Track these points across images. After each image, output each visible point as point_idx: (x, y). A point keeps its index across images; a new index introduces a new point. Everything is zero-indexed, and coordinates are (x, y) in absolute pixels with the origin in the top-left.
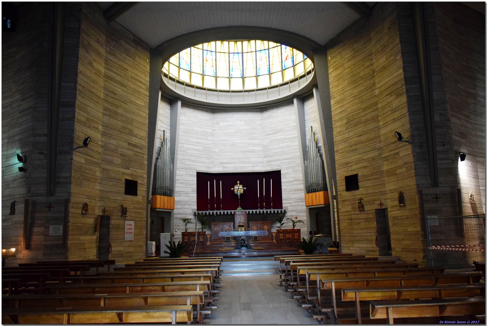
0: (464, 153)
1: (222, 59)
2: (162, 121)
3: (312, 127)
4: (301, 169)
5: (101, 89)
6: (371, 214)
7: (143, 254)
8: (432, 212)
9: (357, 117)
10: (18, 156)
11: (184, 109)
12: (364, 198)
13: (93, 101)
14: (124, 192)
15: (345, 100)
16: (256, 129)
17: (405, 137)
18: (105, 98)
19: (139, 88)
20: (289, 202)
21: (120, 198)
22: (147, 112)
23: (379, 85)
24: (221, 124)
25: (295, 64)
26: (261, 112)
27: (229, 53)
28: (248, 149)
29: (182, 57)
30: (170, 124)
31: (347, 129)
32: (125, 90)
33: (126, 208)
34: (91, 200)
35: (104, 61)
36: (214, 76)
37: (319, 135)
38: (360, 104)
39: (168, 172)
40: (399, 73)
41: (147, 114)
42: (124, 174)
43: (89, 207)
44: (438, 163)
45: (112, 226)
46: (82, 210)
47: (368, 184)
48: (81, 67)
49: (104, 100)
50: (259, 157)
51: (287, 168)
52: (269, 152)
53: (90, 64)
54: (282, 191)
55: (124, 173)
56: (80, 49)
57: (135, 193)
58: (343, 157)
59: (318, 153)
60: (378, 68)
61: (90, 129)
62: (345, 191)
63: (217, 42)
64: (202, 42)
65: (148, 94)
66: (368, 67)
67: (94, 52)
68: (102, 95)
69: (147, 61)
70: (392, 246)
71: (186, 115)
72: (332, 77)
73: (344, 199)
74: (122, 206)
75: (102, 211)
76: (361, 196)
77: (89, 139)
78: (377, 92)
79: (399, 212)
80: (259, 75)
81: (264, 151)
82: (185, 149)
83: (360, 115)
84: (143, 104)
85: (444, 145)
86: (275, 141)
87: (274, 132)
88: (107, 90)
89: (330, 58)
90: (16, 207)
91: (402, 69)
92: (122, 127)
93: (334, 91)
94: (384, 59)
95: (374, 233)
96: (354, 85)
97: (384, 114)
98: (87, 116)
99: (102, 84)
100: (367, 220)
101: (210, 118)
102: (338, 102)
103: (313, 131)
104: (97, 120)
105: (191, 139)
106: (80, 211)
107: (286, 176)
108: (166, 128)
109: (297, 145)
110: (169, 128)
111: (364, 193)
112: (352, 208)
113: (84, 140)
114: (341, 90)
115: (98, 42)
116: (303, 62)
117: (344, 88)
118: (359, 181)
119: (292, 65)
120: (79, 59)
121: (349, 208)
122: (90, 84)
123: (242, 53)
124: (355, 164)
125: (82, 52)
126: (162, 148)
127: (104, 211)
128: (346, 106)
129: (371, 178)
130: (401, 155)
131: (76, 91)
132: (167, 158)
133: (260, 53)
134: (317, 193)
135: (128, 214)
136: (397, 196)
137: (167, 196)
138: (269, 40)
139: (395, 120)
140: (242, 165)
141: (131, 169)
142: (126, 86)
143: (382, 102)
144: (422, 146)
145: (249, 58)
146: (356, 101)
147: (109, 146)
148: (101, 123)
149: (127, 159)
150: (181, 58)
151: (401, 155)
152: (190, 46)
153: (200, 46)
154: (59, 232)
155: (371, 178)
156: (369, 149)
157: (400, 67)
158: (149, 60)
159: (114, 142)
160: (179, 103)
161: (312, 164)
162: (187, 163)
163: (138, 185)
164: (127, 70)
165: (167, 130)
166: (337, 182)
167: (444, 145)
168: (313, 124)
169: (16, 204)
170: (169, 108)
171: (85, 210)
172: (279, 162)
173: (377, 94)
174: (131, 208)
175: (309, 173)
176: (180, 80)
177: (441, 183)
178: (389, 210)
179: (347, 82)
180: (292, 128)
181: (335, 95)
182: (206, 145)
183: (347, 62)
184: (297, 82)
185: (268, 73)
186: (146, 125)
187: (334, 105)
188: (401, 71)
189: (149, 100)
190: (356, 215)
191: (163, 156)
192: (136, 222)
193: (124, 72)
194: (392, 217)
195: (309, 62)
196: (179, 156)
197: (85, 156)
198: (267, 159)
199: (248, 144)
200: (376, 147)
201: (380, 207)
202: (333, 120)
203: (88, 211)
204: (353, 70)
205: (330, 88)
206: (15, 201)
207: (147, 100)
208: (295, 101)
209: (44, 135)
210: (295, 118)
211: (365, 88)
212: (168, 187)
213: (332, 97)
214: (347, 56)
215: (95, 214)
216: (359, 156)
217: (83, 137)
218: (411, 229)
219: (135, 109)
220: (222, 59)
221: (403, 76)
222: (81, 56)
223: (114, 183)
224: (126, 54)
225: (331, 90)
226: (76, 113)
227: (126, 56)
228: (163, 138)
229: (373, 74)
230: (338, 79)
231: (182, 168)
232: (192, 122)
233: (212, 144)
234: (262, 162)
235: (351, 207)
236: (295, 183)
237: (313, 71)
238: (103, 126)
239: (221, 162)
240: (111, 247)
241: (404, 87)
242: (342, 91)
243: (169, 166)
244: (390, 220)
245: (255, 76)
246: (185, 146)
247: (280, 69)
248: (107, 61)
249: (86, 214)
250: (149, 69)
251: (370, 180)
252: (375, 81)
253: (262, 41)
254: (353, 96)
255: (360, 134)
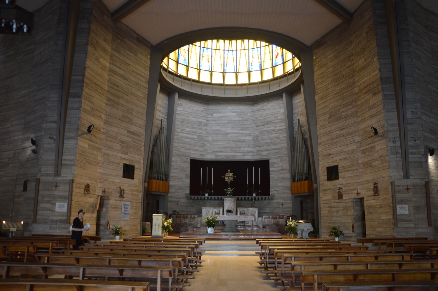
0: (433, 148)
1: (218, 55)
2: (160, 111)
3: (299, 120)
4: (287, 158)
5: (105, 82)
6: (349, 203)
7: (138, 233)
8: (402, 202)
9: (339, 112)
10: (32, 140)
11: (181, 100)
12: (343, 188)
13: (98, 93)
14: (122, 175)
15: (328, 96)
16: (247, 120)
17: (381, 132)
18: (108, 90)
19: (140, 81)
20: (277, 189)
21: (118, 181)
22: (146, 102)
23: (359, 84)
24: (214, 115)
25: (284, 62)
26: (253, 104)
27: (224, 50)
28: (239, 139)
29: (181, 53)
30: (167, 114)
31: (329, 123)
32: (127, 82)
33: (124, 190)
34: (93, 181)
35: (109, 57)
36: (209, 70)
37: (306, 128)
38: (342, 100)
39: (163, 159)
40: (375, 74)
41: (145, 104)
42: (122, 159)
43: (90, 188)
44: (409, 156)
45: (110, 206)
46: (85, 190)
47: (347, 174)
48: (89, 63)
49: (108, 91)
50: (249, 147)
51: (275, 158)
52: (259, 143)
53: (97, 59)
54: (270, 179)
55: (123, 158)
56: (89, 46)
57: (132, 177)
58: (325, 149)
59: (304, 144)
60: (358, 68)
61: (93, 117)
62: (326, 181)
63: (213, 40)
64: (200, 40)
65: (147, 86)
66: (349, 67)
67: (101, 50)
68: (106, 88)
69: (148, 57)
70: (367, 232)
71: (182, 106)
72: (317, 74)
73: (325, 188)
74: (120, 188)
75: (102, 192)
76: (341, 186)
77: (92, 126)
78: (356, 90)
79: (373, 201)
80: (252, 71)
81: (254, 141)
82: (181, 137)
83: (341, 111)
84: (142, 95)
85: (415, 141)
86: (264, 133)
87: (264, 123)
88: (110, 83)
89: (315, 58)
90: (28, 185)
91: (378, 70)
92: (123, 116)
93: (318, 88)
94: (363, 60)
95: (352, 220)
96: (336, 83)
97: (363, 110)
98: (92, 106)
99: (106, 77)
100: (345, 208)
101: (205, 109)
102: (322, 98)
103: (300, 124)
104: (101, 110)
105: (186, 129)
106: (82, 191)
107: (274, 166)
108: (163, 117)
109: (284, 136)
110: (166, 117)
111: (344, 183)
112: (332, 197)
113: (88, 127)
114: (325, 87)
115: (105, 40)
116: (292, 60)
117: (328, 85)
118: (339, 172)
119: (282, 62)
120: (88, 56)
121: (329, 197)
122: (96, 77)
123: (236, 50)
124: (336, 156)
125: (90, 49)
126: (159, 136)
127: (104, 192)
128: (329, 102)
129: (350, 169)
130: (377, 149)
131: (83, 84)
132: (163, 145)
133: (253, 50)
134: (302, 182)
135: (125, 195)
136: (372, 186)
137: (162, 180)
138: (261, 40)
139: (372, 117)
140: (233, 154)
141: (129, 154)
142: (128, 79)
143: (361, 99)
144: (395, 141)
145: (242, 56)
146: (338, 97)
147: (110, 133)
148: (104, 112)
149: (126, 145)
150: (179, 54)
151: (377, 149)
152: (188, 44)
153: (198, 44)
154: (63, 209)
155: (350, 169)
156: (348, 142)
157: (377, 69)
158: (150, 56)
159: (115, 130)
160: (177, 95)
161: (299, 154)
162: (181, 150)
163: (135, 169)
164: (129, 65)
165: (164, 119)
166: (320, 172)
167: (415, 141)
168: (301, 117)
169: (28, 182)
170: (167, 99)
171: (87, 190)
172: (268, 152)
173: (356, 92)
174: (128, 190)
175: (296, 163)
176: (178, 74)
177: (411, 176)
178: (365, 199)
179: (330, 80)
180: (281, 120)
181: (319, 91)
182: (201, 135)
183: (330, 61)
184: (286, 78)
185: (260, 69)
186: (145, 115)
187: (319, 100)
188: (377, 72)
189: (148, 92)
190: (336, 204)
191: (160, 143)
192: (132, 203)
193: (127, 67)
194: (367, 206)
195: (297, 60)
196: (175, 144)
197: (89, 142)
198: (257, 149)
199: (239, 134)
200: (355, 140)
201: (357, 196)
202: (317, 114)
203: (89, 191)
204: (335, 69)
205: (315, 85)
206: (27, 180)
207: (146, 91)
208: (284, 95)
209: (55, 122)
210: (284, 112)
211: (346, 85)
212: (163, 172)
213: (317, 93)
214: (330, 56)
215: (95, 194)
216: (339, 148)
217: (87, 125)
218: (384, 217)
219: (135, 100)
220: (218, 55)
221: (379, 76)
222: (89, 52)
223: (114, 167)
224: (129, 51)
225: (315, 87)
226: (82, 103)
227: (129, 53)
228: (160, 127)
229: (353, 73)
230: (322, 77)
231: (177, 155)
232: (187, 113)
233: (205, 134)
234: (252, 152)
235: (331, 196)
236: (282, 172)
237: (300, 69)
238: (105, 115)
239: (214, 150)
240: (109, 225)
241: (380, 86)
242: (325, 88)
243: (165, 153)
244: (366, 208)
245: (247, 72)
246: (180, 134)
247: (271, 66)
248: (112, 57)
249: (88, 194)
250: (149, 64)
251: (349, 171)
252: (354, 80)
253: (255, 41)
254: (335, 92)
255: (341, 128)
